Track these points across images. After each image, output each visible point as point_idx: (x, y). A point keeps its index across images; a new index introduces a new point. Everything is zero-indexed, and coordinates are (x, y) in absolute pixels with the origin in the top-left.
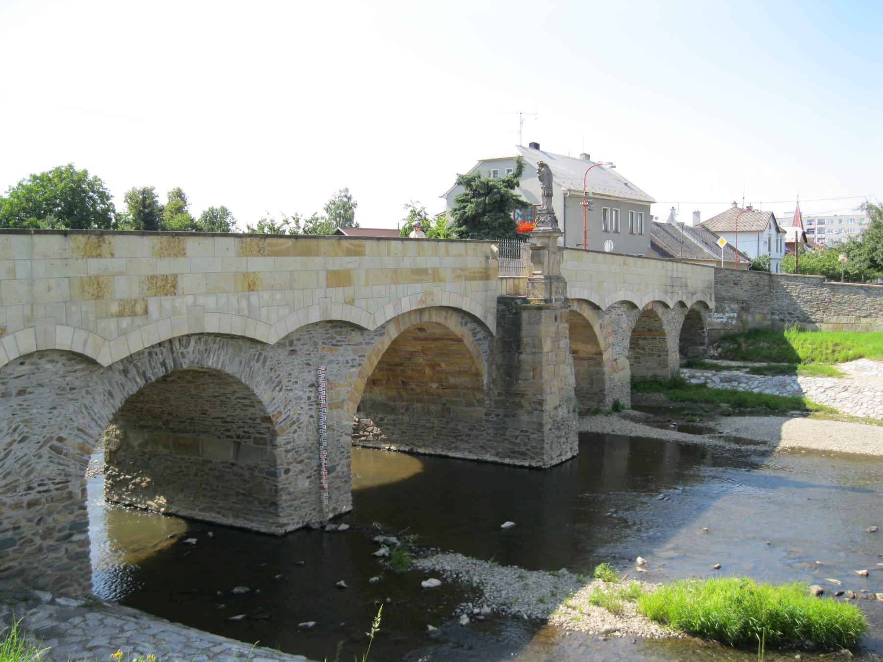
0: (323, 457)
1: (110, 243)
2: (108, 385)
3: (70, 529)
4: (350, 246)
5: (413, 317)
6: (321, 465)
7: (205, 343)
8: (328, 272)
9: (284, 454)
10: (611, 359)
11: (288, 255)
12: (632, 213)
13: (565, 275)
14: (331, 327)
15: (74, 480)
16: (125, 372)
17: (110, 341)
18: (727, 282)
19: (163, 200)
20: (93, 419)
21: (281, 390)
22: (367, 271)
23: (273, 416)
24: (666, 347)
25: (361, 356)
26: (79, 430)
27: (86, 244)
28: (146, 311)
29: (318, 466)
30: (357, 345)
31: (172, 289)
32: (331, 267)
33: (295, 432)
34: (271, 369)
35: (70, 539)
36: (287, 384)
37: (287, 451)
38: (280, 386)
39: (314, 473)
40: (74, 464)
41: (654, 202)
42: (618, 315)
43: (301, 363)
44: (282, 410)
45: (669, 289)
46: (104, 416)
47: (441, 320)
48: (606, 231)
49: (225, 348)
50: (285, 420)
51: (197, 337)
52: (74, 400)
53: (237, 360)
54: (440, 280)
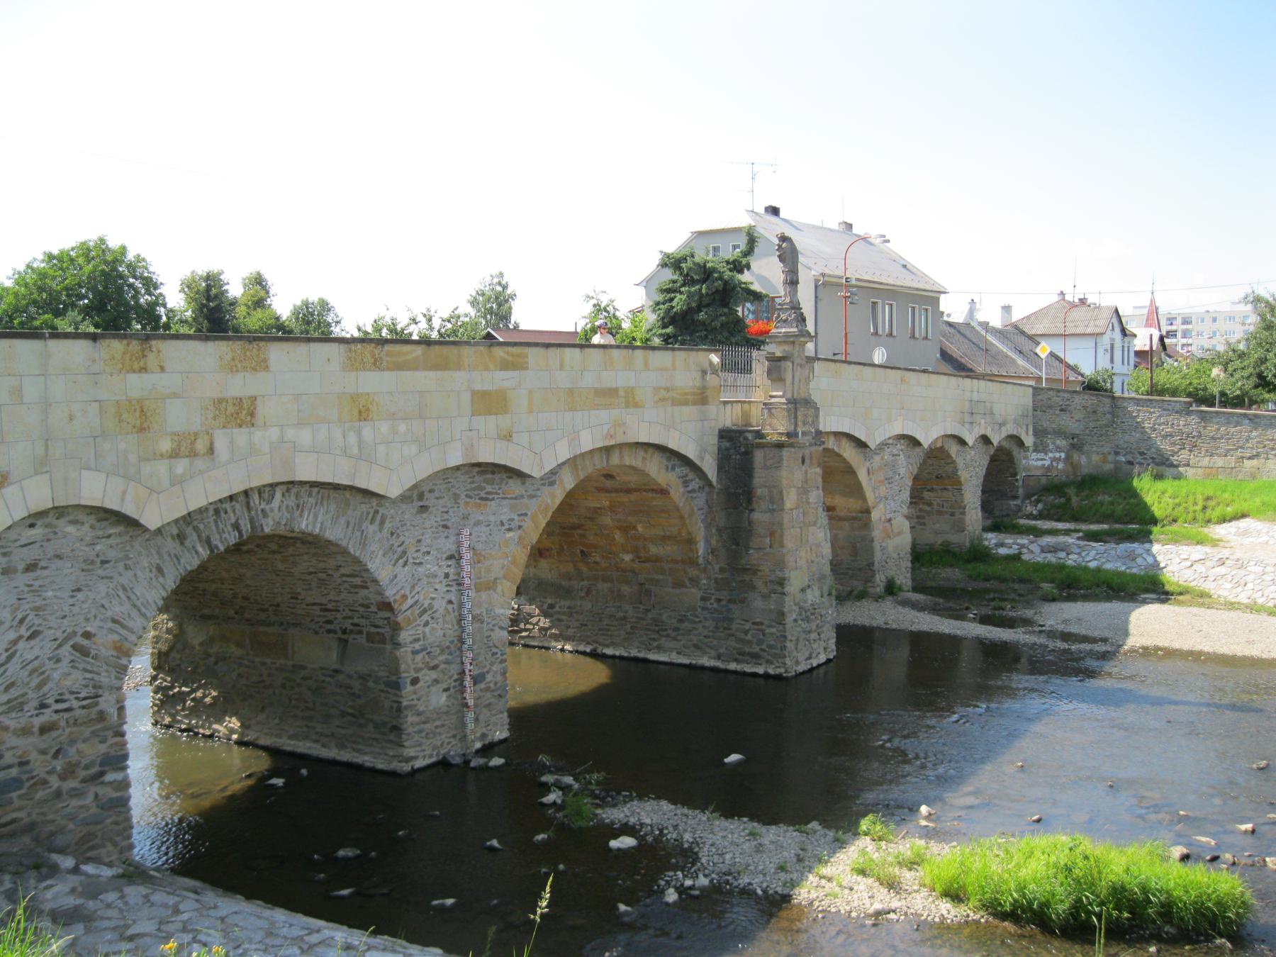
0: (467, 661)
1: (159, 352)
2: (156, 557)
3: (101, 765)
4: (506, 356)
5: (596, 458)
6: (463, 672)
7: (297, 496)
8: (474, 393)
9: (410, 656)
10: (883, 519)
11: (416, 369)
12: (913, 308)
13: (816, 397)
14: (479, 473)
15: (107, 694)
16: (181, 538)
17: (158, 493)
18: (1050, 407)
19: (235, 289)
20: (134, 606)
21: (405, 564)
22: (531, 392)
23: (395, 601)
24: (962, 502)
25: (522, 515)
26: (114, 621)
27: (124, 353)
28: (211, 450)
29: (460, 674)
30: (515, 498)
31: (249, 418)
32: (478, 386)
33: (426, 624)
34: (392, 534)
35: (101, 779)
36: (415, 555)
37: (415, 652)
38: (405, 559)
39: (454, 684)
40: (107, 671)
41: (945, 293)
42: (894, 455)
43: (435, 524)
44: (408, 593)
45: (967, 418)
46: (151, 601)
47: (638, 463)
48: (876, 333)
49: (325, 503)
50: (411, 606)
51: (284, 487)
52: (107, 578)
53: (342, 521)
54: (636, 405)
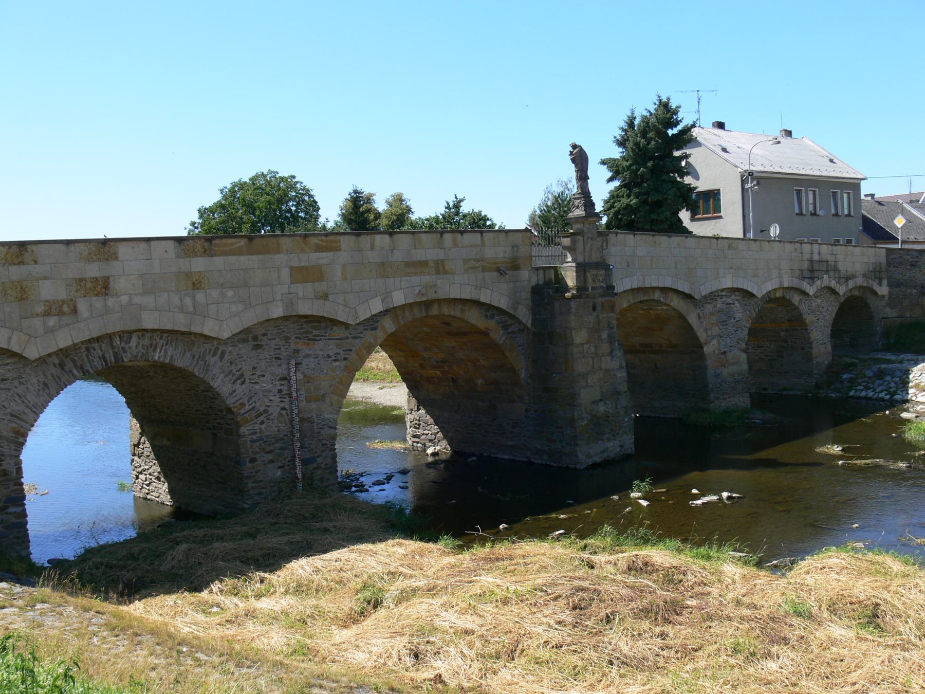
0: (297, 448)
1: (32, 252)
2: (42, 377)
3: (5, 502)
4: (320, 243)
5: (416, 310)
6: (294, 457)
7: (151, 338)
8: (292, 268)
9: (249, 444)
10: (717, 352)
11: (240, 254)
12: (814, 191)
13: (611, 261)
14: (306, 322)
15: (8, 459)
16: (62, 365)
17: (36, 338)
18: (901, 263)
19: (381, 205)
20: (27, 407)
21: (243, 383)
22: (344, 266)
23: (234, 407)
24: (810, 338)
25: (347, 350)
26: (12, 415)
27: (7, 254)
29: (293, 457)
30: (341, 339)
31: (104, 290)
32: (295, 263)
33: (262, 423)
34: (231, 363)
35: (5, 511)
36: (251, 377)
37: (253, 441)
38: (242, 379)
39: (287, 463)
40: (8, 445)
41: (864, 179)
42: (727, 304)
43: (269, 357)
44: (246, 402)
45: (807, 274)
46: (39, 404)
47: (458, 314)
48: (801, 214)
49: (174, 343)
50: (248, 411)
51: (140, 334)
52: (6, 389)
53: (188, 354)
54: (446, 273)
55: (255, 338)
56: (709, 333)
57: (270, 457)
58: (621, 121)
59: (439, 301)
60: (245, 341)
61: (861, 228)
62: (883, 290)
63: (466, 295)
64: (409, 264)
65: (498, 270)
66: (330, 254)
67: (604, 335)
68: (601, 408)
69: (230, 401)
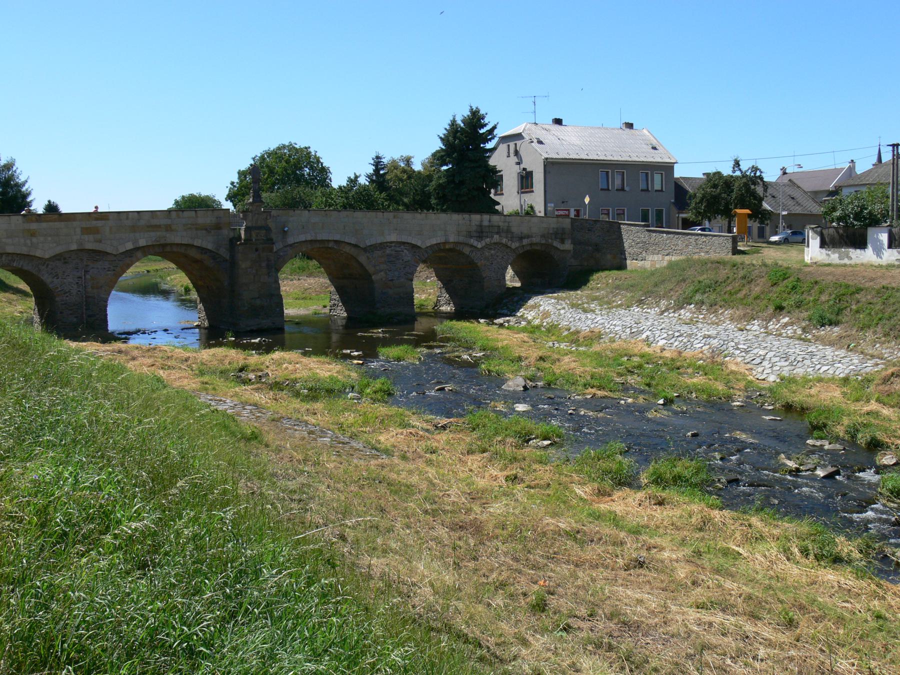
8: (82, 228)
10: (384, 279)
11: (55, 221)
32: (84, 226)
37: (62, 304)
55: (65, 259)
56: (378, 268)
57: (70, 312)
58: (442, 128)
59: (172, 245)
60: (59, 260)
61: (673, 201)
62: (568, 246)
63: (185, 241)
64: (148, 226)
65: (206, 229)
66: (103, 222)
67: (264, 264)
68: (258, 302)
69: (50, 286)
